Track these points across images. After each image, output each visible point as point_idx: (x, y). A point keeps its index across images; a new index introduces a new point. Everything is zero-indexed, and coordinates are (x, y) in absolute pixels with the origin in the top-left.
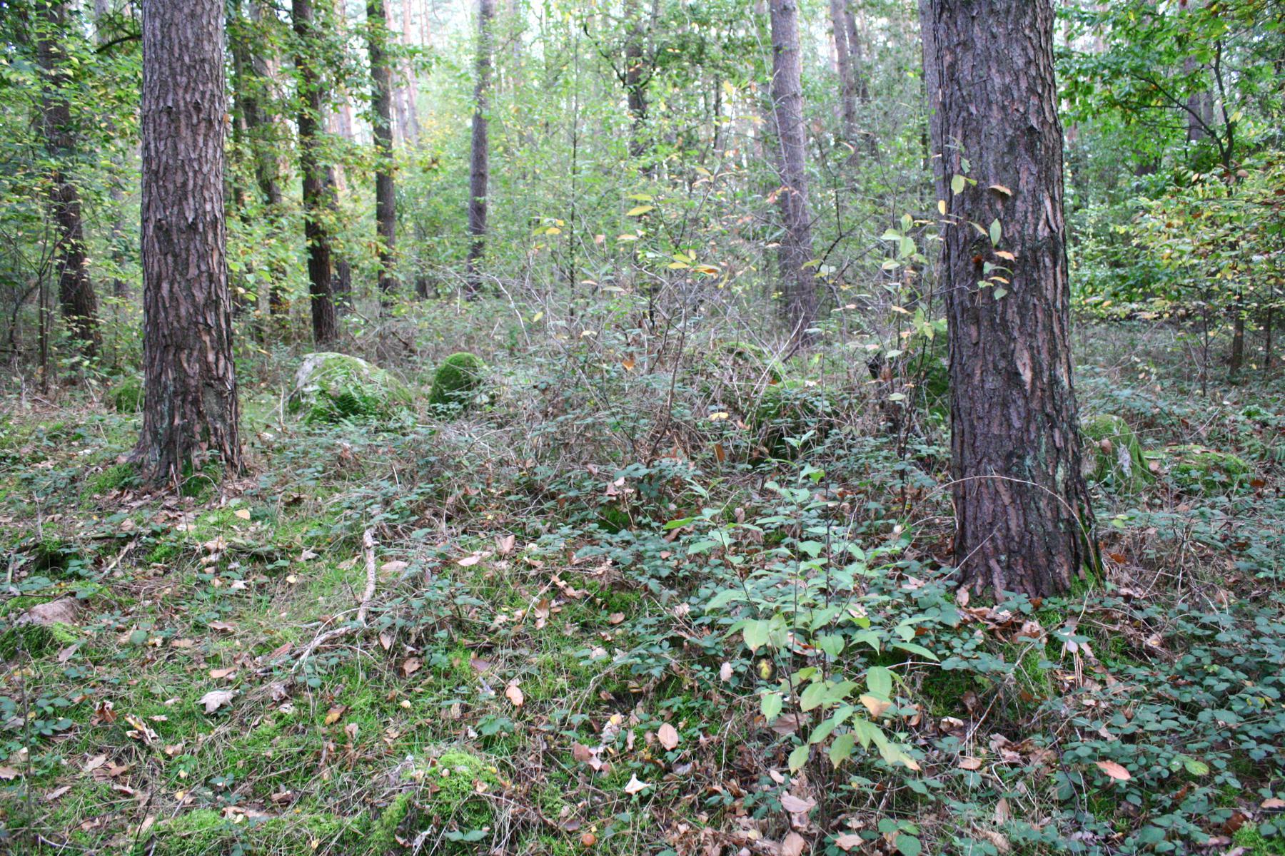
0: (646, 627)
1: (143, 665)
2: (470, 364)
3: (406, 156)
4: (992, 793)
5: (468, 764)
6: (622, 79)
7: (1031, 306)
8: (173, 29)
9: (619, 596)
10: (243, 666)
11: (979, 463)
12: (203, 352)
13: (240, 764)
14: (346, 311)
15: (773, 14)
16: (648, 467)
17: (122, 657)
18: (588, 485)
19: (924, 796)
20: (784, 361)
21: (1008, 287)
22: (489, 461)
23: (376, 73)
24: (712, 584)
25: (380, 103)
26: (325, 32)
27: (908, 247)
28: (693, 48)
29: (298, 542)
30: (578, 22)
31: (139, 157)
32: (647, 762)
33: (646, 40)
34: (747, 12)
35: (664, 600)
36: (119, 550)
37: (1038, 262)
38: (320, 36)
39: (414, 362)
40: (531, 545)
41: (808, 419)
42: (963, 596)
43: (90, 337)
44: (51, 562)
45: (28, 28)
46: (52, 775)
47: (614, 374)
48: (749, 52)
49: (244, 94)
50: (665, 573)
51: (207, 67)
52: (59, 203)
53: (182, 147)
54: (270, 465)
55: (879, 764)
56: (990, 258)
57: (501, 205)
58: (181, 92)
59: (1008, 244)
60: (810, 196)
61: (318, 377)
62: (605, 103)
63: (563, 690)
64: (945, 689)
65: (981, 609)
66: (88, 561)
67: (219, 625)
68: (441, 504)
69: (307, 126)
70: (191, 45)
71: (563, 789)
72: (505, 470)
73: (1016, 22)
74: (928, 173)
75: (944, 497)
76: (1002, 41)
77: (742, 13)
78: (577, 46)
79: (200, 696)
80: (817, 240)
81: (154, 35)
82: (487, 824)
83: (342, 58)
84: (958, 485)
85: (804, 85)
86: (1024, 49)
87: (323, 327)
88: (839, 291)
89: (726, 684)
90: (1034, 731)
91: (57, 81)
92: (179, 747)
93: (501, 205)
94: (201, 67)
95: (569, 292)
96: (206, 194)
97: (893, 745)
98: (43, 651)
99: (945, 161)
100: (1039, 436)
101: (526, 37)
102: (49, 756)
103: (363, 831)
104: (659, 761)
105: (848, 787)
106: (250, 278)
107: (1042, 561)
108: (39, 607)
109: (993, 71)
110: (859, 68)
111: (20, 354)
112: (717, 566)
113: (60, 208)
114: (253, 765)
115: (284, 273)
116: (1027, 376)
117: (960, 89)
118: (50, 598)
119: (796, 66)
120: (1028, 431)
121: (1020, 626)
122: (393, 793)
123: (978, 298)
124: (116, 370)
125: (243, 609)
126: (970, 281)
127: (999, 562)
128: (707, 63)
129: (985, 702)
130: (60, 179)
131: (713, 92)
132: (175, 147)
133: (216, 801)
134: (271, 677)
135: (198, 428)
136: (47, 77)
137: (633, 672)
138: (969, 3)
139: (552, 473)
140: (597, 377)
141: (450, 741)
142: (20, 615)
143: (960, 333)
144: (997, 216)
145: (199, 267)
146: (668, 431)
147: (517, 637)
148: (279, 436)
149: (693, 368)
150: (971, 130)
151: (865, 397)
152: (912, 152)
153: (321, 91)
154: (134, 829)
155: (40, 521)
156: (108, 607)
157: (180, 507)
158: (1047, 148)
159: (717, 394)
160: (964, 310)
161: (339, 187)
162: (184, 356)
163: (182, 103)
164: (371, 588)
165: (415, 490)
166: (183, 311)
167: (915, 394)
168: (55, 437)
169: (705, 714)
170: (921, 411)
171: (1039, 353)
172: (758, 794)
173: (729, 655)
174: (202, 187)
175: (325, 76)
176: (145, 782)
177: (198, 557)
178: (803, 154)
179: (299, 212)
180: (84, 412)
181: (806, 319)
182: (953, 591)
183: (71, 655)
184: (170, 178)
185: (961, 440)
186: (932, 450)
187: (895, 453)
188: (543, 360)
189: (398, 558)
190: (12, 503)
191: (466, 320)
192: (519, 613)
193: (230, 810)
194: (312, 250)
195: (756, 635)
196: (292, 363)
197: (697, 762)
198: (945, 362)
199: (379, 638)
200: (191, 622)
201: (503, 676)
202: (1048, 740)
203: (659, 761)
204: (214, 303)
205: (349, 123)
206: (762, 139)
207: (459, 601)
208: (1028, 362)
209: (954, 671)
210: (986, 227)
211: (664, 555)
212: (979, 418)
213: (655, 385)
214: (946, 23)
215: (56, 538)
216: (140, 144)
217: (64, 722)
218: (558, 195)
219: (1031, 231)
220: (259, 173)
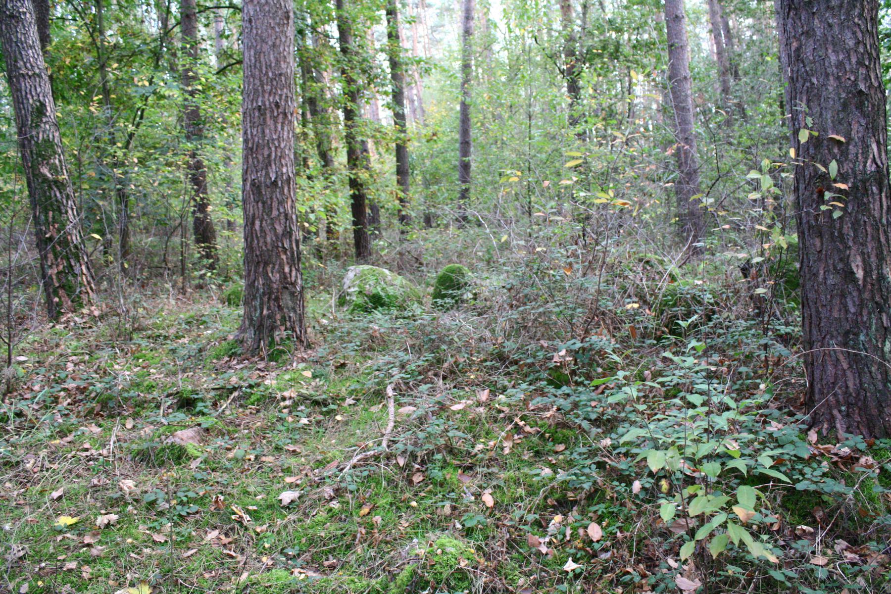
0: (580, 454)
1: (242, 473)
2: (460, 272)
3: (415, 131)
4: (837, 584)
5: (455, 546)
6: (562, 72)
7: (862, 223)
8: (262, 55)
9: (561, 433)
10: (306, 475)
11: (824, 338)
12: (281, 266)
13: (304, 540)
14: (376, 237)
15: (667, 21)
16: (582, 342)
17: (229, 467)
18: (541, 355)
19: (782, 583)
20: (680, 267)
21: (844, 209)
22: (472, 338)
23: (395, 77)
24: (627, 425)
25: (398, 97)
26: (360, 51)
27: (767, 182)
28: (611, 49)
29: (344, 392)
30: (530, 35)
31: (241, 139)
32: (580, 549)
33: (578, 44)
34: (650, 21)
35: (593, 435)
36: (228, 397)
37: (867, 190)
38: (357, 53)
39: (423, 271)
40: (501, 396)
41: (696, 308)
42: (813, 436)
43: (212, 257)
44: (187, 403)
45: (177, 62)
46: (186, 542)
47: (558, 278)
48: (651, 49)
49: (308, 95)
50: (593, 416)
51: (283, 78)
52: (193, 172)
53: (267, 131)
54: (325, 341)
55: (748, 557)
56: (829, 189)
57: (481, 163)
58: (267, 96)
59: (843, 178)
60: (698, 149)
61: (357, 282)
62: (550, 90)
63: (521, 497)
64: (799, 505)
65: (827, 446)
66: (209, 403)
67: (291, 448)
68: (439, 368)
69: (349, 114)
70: (273, 65)
71: (520, 566)
72: (483, 344)
73: (848, 14)
74: (785, 129)
75: (798, 363)
76: (836, 29)
77: (646, 22)
78: (529, 52)
79: (278, 494)
80: (703, 180)
81: (250, 60)
82: (466, 588)
83: (371, 68)
84: (808, 354)
85: (692, 70)
86: (854, 33)
87: (361, 249)
88: (718, 216)
89: (637, 496)
90: (870, 539)
91: (192, 94)
92: (264, 527)
93: (481, 163)
94: (278, 79)
95: (528, 221)
96: (283, 162)
97: (758, 544)
98: (181, 461)
99: (793, 119)
100: (870, 319)
101: (496, 47)
102: (187, 529)
103: (383, 589)
104: (588, 549)
105: (725, 573)
106: (312, 217)
107: (875, 412)
108: (179, 432)
109: (830, 51)
110: (732, 56)
111: (169, 269)
112: (631, 412)
113: (193, 175)
114: (312, 542)
115: (335, 212)
116: (860, 274)
117: (804, 66)
118: (186, 427)
119: (686, 57)
120: (861, 314)
121: (858, 459)
122: (404, 564)
123: (820, 218)
124: (227, 279)
125: (307, 437)
126: (814, 206)
127: (840, 411)
128: (622, 58)
129: (830, 515)
130: (193, 156)
131: (627, 78)
132: (263, 132)
133: (288, 564)
134: (324, 483)
135: (278, 317)
136: (186, 91)
137: (570, 486)
138: (810, 3)
139: (515, 346)
140: (547, 279)
141: (443, 530)
142: (167, 437)
143: (808, 244)
144: (834, 157)
145: (278, 210)
146: (597, 316)
147: (490, 460)
148: (331, 321)
149: (614, 272)
150: (813, 96)
151: (738, 292)
152: (772, 114)
153: (358, 90)
154: (236, 580)
155: (180, 377)
156: (221, 434)
157: (266, 369)
158: (873, 105)
159: (631, 290)
160: (810, 227)
161: (371, 154)
162: (269, 269)
163: (267, 103)
164: (391, 424)
165: (422, 358)
166: (269, 239)
167: (775, 289)
168: (189, 322)
169: (622, 517)
170: (780, 301)
171: (869, 257)
172: (659, 576)
173: (639, 476)
174: (280, 157)
175: (361, 81)
176: (243, 549)
177: (278, 402)
178: (692, 120)
179: (345, 172)
180: (208, 306)
181: (695, 237)
182: (805, 432)
183: (198, 465)
184: (260, 152)
185: (809, 322)
186: (789, 329)
187: (761, 332)
188: (509, 268)
189: (410, 404)
190: (163, 365)
191: (457, 242)
192: (492, 443)
193: (296, 571)
194: (353, 197)
195: (656, 461)
196: (341, 272)
197: (615, 551)
198: (797, 265)
199: (396, 459)
200: (273, 445)
201: (480, 487)
202: (881, 546)
203: (588, 549)
204: (288, 234)
205: (377, 111)
206: (663, 110)
207: (450, 434)
208: (860, 264)
209: (806, 491)
210: (826, 167)
211: (593, 404)
212: (824, 306)
213: (587, 285)
214: (793, 19)
215: (190, 388)
216: (241, 132)
217: (194, 508)
218: (519, 154)
219: (861, 168)
220: (319, 146)
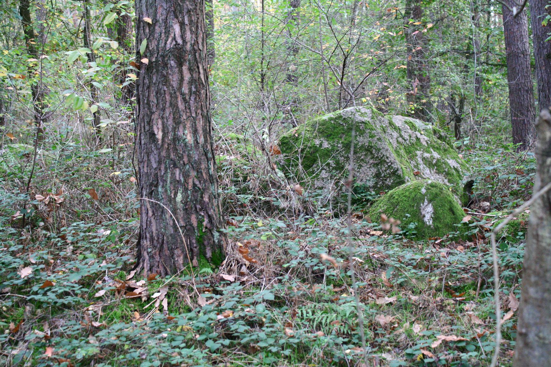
7: (162, 91)
100: (166, 172)
219: (163, 45)
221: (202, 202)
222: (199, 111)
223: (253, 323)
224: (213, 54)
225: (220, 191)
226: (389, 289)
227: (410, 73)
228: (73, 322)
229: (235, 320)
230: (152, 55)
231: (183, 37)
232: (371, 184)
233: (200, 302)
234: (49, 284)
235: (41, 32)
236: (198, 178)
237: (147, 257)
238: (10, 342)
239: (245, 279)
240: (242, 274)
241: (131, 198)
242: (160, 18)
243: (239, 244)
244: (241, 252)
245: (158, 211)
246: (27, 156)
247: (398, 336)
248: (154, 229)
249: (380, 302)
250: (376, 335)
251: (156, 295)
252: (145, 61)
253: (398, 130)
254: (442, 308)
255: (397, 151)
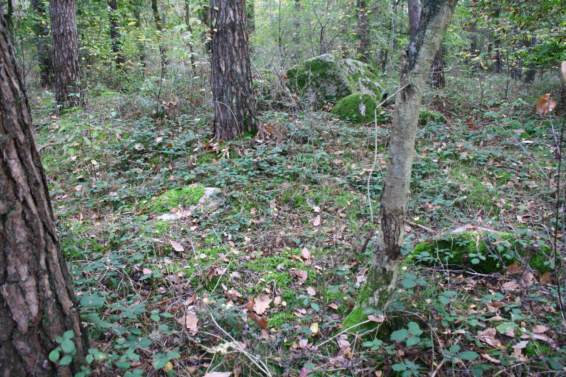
12: (67, 72)
53: (58, 9)
96: (67, 24)
100: (227, 88)
132: (56, 10)
162: (62, 74)
166: (61, 60)
204: (71, 58)
221: (246, 103)
222: (244, 56)
223: (271, 163)
224: (254, 27)
225: (256, 98)
226: (341, 147)
227: (359, 37)
228: (183, 163)
229: (262, 161)
230: (219, 27)
231: (235, 17)
232: (334, 94)
233: (245, 153)
234: (170, 145)
235: (163, 18)
236: (243, 91)
237: (219, 131)
238: (153, 173)
239: (268, 142)
240: (267, 140)
241: (210, 102)
242: (223, 7)
243: (265, 125)
244: (266, 129)
245: (224, 108)
246: (157, 82)
247: (343, 169)
248: (222, 117)
249: (335, 153)
250: (333, 169)
251: (223, 150)
252: (215, 30)
253: (349, 66)
254: (366, 156)
255: (348, 78)
